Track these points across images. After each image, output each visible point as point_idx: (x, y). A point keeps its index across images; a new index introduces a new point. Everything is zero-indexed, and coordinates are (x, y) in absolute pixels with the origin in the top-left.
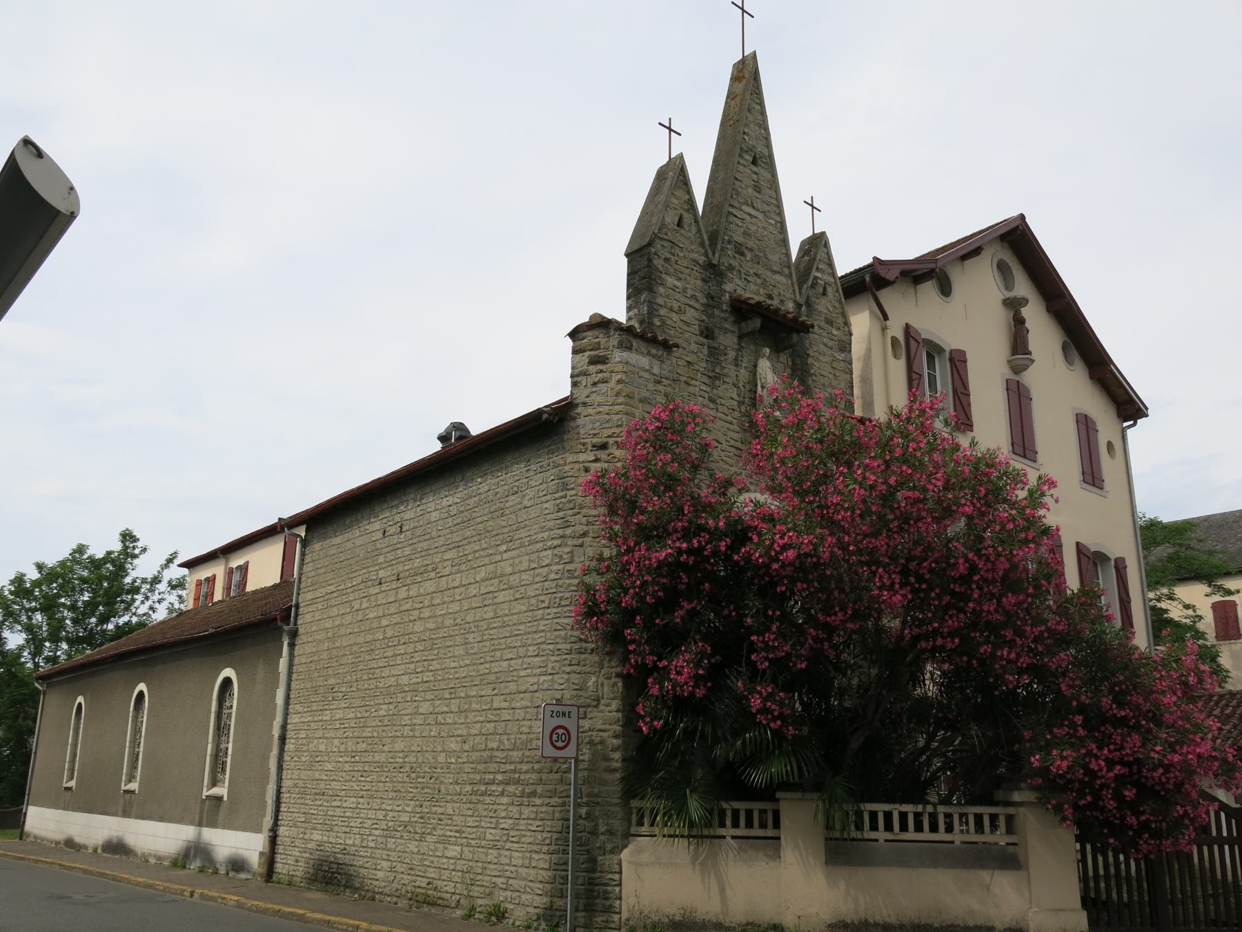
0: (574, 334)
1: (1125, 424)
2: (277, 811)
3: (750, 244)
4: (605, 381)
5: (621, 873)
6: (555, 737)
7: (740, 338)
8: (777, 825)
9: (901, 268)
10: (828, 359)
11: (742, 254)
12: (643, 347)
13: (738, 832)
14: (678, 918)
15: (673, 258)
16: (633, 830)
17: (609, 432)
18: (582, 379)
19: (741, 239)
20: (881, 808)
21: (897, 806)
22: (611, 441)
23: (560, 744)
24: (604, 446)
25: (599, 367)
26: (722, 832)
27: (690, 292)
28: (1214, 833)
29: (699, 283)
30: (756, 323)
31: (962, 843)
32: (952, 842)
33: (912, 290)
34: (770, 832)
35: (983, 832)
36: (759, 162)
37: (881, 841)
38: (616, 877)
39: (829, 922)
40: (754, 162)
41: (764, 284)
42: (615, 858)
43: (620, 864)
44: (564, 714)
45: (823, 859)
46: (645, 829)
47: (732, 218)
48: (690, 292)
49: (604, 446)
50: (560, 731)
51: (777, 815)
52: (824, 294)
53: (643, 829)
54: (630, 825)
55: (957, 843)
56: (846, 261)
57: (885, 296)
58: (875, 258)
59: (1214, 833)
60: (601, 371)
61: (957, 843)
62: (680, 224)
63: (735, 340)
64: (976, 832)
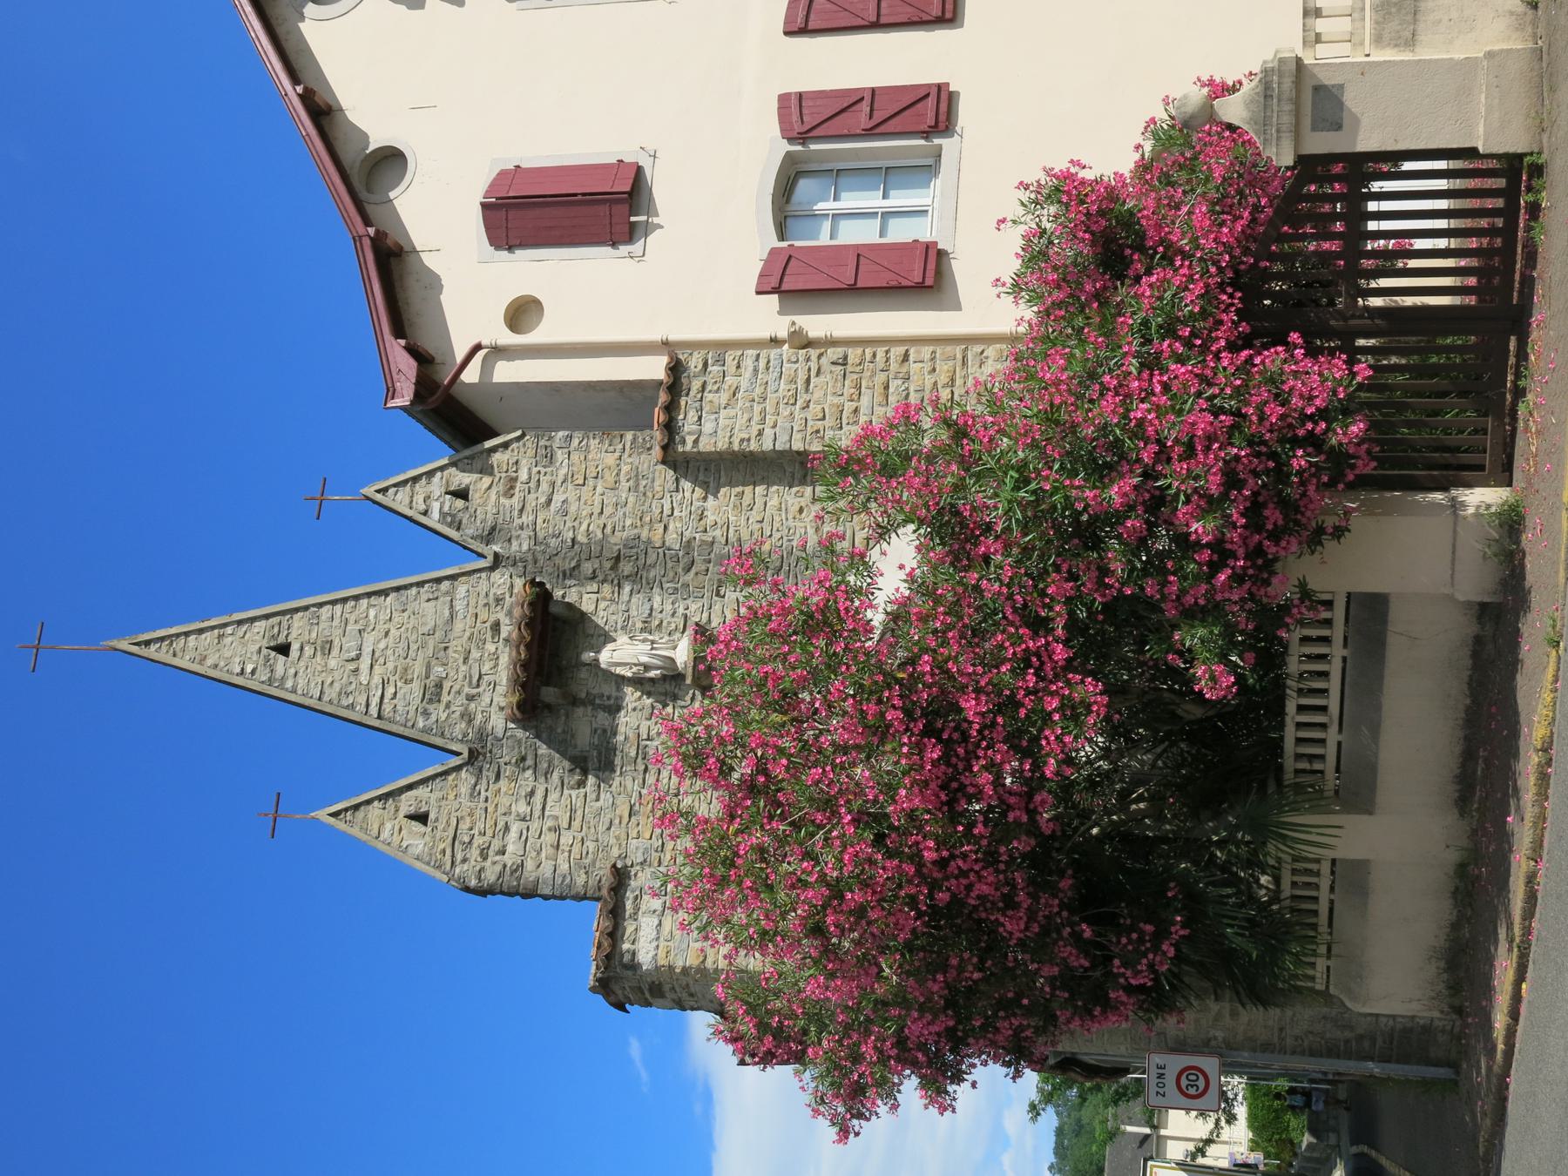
0: (621, 1007)
3: (418, 669)
5: (1377, 1015)
6: (1192, 1091)
7: (575, 702)
10: (571, 494)
11: (439, 686)
13: (1323, 928)
14: (1442, 964)
15: (478, 841)
16: (1320, 987)
19: (416, 688)
20: (1290, 733)
21: (1288, 719)
23: (1201, 1083)
26: (1323, 908)
27: (522, 808)
29: (503, 784)
30: (549, 694)
31: (1345, 645)
32: (1344, 659)
33: (412, 257)
34: (1325, 868)
35: (1326, 691)
36: (281, 639)
37: (1340, 738)
39: (1457, 816)
41: (477, 640)
44: (1160, 1076)
45: (1365, 817)
47: (387, 708)
48: (522, 808)
50: (1184, 1082)
53: (1318, 975)
54: (1312, 990)
55: (1345, 652)
61: (1345, 652)
62: (422, 818)
63: (580, 711)
64: (1329, 662)
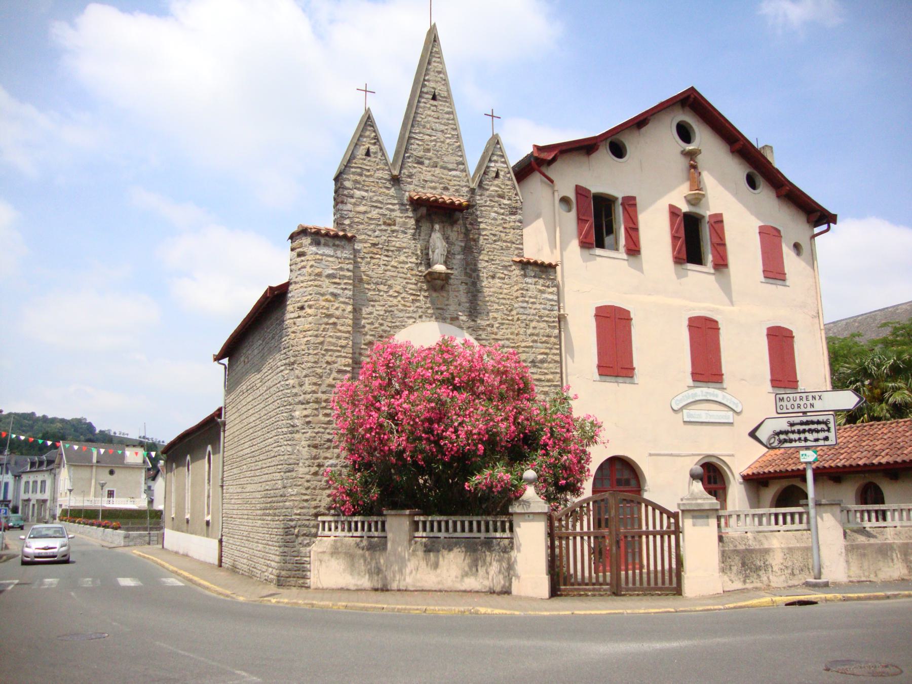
1: (817, 230)
2: (819, 547)
4: (304, 267)
8: (383, 530)
9: (560, 148)
11: (422, 163)
12: (331, 242)
17: (305, 299)
18: (293, 267)
22: (306, 304)
24: (302, 308)
25: (303, 258)
28: (592, 538)
36: (438, 97)
38: (308, 559)
40: (434, 98)
42: (308, 549)
43: (310, 552)
46: (327, 532)
49: (302, 308)
51: (383, 523)
52: (497, 176)
56: (518, 149)
57: (551, 172)
58: (535, 146)
59: (592, 538)
60: (303, 261)
